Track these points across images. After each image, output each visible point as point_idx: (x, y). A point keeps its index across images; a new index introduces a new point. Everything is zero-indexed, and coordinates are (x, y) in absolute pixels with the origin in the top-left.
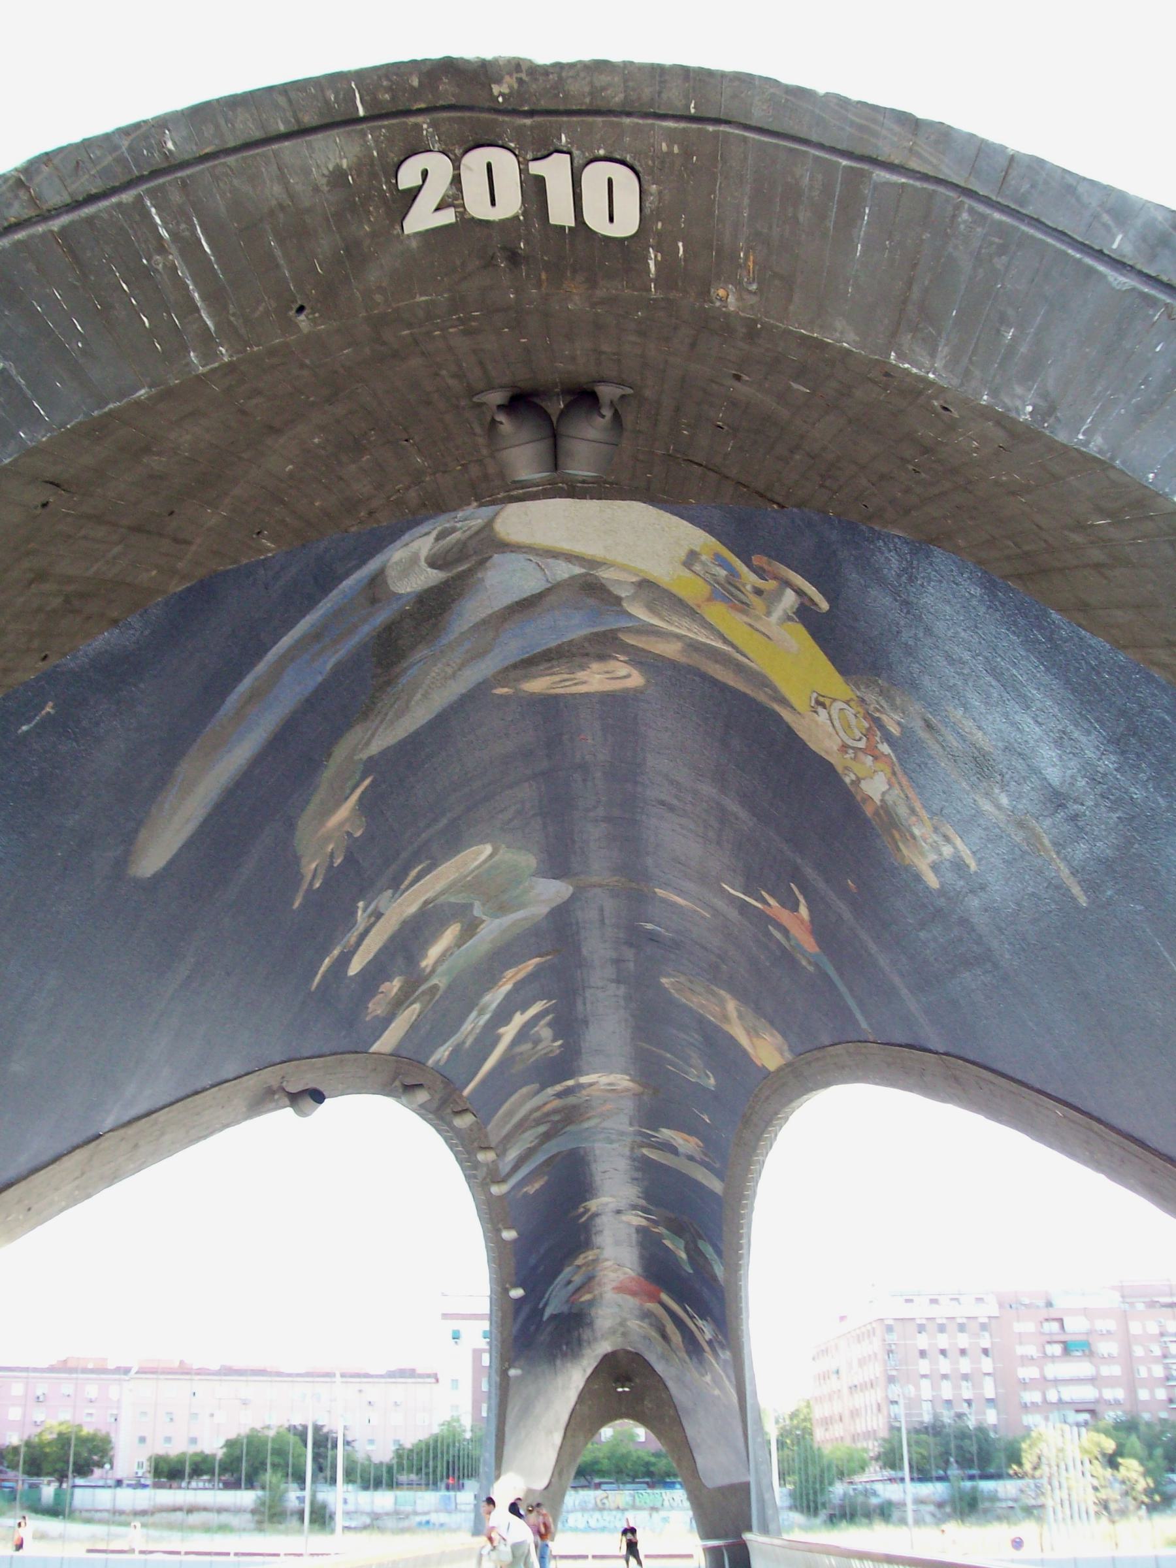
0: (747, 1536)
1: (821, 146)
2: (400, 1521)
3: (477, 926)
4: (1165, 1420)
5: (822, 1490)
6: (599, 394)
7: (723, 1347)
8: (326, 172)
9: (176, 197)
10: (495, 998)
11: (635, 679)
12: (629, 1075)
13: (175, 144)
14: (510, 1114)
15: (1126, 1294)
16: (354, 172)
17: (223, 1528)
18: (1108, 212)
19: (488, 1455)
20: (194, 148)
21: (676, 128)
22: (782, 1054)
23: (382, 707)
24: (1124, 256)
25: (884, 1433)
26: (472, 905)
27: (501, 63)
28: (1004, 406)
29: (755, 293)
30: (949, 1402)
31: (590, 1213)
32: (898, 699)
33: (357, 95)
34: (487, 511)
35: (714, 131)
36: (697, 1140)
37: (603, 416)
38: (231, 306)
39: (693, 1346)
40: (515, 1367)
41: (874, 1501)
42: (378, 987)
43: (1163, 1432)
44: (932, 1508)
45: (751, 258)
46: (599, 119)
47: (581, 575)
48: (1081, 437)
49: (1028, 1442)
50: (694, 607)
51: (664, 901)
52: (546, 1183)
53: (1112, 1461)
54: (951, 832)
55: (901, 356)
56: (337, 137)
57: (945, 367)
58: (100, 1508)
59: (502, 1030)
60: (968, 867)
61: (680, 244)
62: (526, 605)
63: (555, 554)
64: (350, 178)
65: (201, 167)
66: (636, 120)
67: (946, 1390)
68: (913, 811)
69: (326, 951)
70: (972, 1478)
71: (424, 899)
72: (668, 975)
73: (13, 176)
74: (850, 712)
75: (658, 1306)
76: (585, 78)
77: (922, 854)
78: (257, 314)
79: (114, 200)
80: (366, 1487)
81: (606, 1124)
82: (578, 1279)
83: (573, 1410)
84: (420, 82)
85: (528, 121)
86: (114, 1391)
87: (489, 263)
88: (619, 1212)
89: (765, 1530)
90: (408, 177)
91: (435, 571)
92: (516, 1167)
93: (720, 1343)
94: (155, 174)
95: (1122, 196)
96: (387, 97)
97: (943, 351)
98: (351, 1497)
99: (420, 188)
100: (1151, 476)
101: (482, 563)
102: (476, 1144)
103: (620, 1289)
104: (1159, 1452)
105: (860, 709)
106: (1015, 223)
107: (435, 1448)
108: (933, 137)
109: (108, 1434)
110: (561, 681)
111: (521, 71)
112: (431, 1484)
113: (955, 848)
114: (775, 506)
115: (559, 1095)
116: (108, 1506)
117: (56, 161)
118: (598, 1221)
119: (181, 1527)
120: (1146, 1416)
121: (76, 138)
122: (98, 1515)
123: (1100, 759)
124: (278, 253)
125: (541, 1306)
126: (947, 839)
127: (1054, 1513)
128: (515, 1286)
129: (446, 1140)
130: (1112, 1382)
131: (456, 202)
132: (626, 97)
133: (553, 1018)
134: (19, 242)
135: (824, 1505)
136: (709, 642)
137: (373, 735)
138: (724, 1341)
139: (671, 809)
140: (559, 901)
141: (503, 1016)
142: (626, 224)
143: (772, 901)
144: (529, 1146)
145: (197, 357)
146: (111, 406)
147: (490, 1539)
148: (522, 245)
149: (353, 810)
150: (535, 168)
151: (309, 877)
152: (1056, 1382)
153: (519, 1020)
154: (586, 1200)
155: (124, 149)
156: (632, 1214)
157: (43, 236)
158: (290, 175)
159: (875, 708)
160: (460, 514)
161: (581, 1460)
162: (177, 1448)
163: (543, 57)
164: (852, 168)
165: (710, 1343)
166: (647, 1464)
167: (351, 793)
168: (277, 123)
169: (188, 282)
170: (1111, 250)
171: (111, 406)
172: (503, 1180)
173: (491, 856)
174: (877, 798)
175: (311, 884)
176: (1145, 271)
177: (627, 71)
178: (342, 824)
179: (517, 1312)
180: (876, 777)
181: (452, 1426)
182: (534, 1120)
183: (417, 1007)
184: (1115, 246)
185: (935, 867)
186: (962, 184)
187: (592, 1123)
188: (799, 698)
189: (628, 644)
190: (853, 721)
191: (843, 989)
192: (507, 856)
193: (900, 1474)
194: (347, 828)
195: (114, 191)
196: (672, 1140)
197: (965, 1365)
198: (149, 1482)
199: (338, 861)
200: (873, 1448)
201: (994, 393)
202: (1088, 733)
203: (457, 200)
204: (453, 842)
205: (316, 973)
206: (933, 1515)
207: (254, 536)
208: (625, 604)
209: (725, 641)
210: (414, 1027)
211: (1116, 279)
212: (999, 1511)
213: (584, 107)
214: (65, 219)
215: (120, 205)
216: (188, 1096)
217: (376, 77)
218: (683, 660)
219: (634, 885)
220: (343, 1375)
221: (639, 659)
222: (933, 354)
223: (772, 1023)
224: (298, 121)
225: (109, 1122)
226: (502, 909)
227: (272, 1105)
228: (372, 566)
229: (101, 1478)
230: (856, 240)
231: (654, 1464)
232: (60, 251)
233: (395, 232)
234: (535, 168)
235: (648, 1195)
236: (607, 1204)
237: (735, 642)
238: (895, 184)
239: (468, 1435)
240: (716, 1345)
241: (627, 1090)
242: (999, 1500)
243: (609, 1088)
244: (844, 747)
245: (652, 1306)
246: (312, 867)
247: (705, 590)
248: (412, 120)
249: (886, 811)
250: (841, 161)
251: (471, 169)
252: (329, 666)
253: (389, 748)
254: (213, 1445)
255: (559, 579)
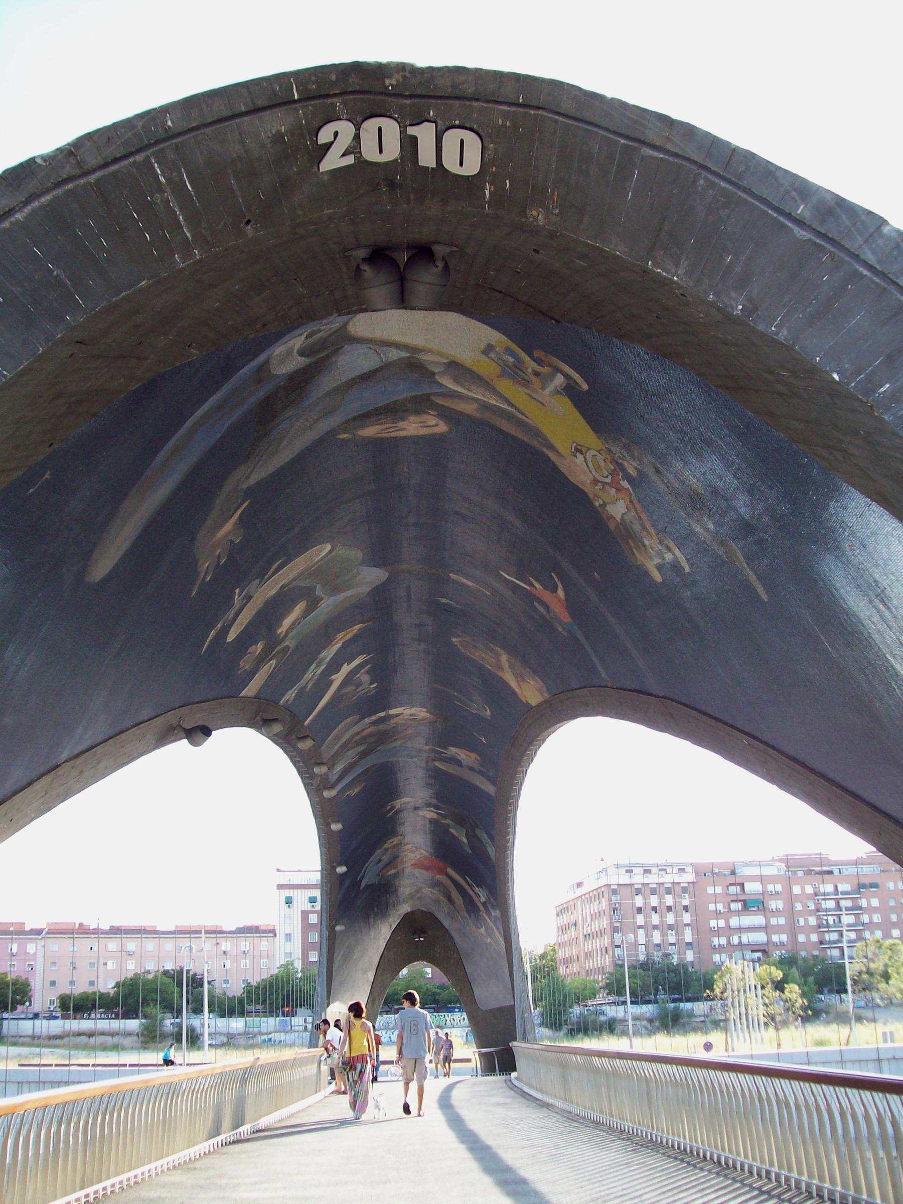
0: (513, 1044)
1: (607, 130)
2: (248, 1040)
3: (318, 602)
4: (817, 956)
5: (564, 1011)
6: (434, 251)
7: (494, 907)
8: (270, 135)
9: (171, 156)
10: (328, 654)
11: (442, 427)
12: (426, 708)
13: (172, 122)
14: (338, 738)
15: (790, 863)
16: (288, 134)
17: (116, 1048)
18: (795, 190)
19: (321, 989)
20: (185, 124)
21: (509, 110)
22: (542, 694)
23: (259, 452)
24: (805, 218)
25: (610, 969)
26: (315, 587)
27: (392, 66)
28: (724, 303)
29: (557, 215)
30: (658, 945)
31: (395, 809)
32: (636, 452)
33: (294, 86)
34: (345, 318)
35: (534, 114)
36: (476, 756)
37: (437, 267)
38: (203, 223)
39: (471, 907)
40: (339, 924)
41: (602, 1018)
42: (247, 649)
43: (815, 965)
44: (645, 1023)
45: (556, 193)
46: (457, 103)
47: (408, 358)
48: (773, 329)
49: (719, 973)
50: (489, 380)
51: (455, 582)
52: (363, 788)
53: (779, 986)
54: (672, 544)
55: (655, 264)
56: (279, 113)
57: (685, 274)
58: (23, 1034)
59: (333, 677)
60: (683, 569)
61: (508, 181)
62: (367, 377)
63: (389, 344)
64: (286, 138)
65: (189, 135)
66: (482, 104)
67: (657, 938)
68: (644, 528)
69: (212, 626)
70: (674, 1001)
71: (281, 584)
72: (457, 636)
73: (66, 148)
74: (600, 458)
75: (445, 877)
76: (448, 77)
77: (650, 558)
78: (219, 227)
79: (131, 160)
80: (223, 1016)
81: (409, 744)
82: (386, 858)
83: (382, 954)
84: (337, 78)
85: (408, 102)
86: (31, 948)
87: (376, 188)
88: (416, 808)
89: (525, 1040)
90: (324, 136)
91: (303, 358)
92: (340, 779)
93: (492, 904)
94: (158, 142)
95: (804, 181)
96: (314, 87)
97: (684, 263)
98: (212, 1022)
99: (332, 143)
100: (818, 358)
101: (336, 352)
102: (312, 761)
103: (418, 865)
104: (811, 979)
105: (608, 457)
106: (735, 190)
107: (277, 984)
108: (682, 131)
109: (27, 979)
110: (386, 429)
111: (406, 71)
112: (272, 1011)
113: (674, 554)
114: (553, 321)
115: (374, 723)
116: (30, 1032)
117: (95, 138)
118: (401, 816)
119: (85, 1047)
120: (803, 954)
121: (109, 122)
122: (22, 1040)
123: (778, 505)
124: (235, 187)
125: (359, 878)
126: (669, 549)
127: (735, 1025)
128: (340, 864)
129: (291, 758)
130: (779, 929)
131: (355, 151)
132: (476, 90)
133: (371, 667)
134: (69, 190)
135: (566, 1021)
136: (498, 404)
137: (252, 471)
138: (495, 903)
139: (464, 517)
140: (378, 583)
141: (334, 666)
142: (472, 166)
143: (537, 585)
144: (350, 761)
145: (179, 257)
146: (124, 294)
147: (327, 1049)
148: (398, 177)
149: (235, 524)
150: (411, 131)
151: (202, 575)
152: (740, 930)
153: (346, 669)
154: (393, 800)
155: (139, 127)
156: (427, 810)
157: (84, 186)
158: (247, 138)
159: (619, 456)
160: (325, 321)
161: (389, 990)
162: (81, 988)
163: (421, 62)
164: (627, 145)
165: (484, 904)
166: (434, 994)
167: (234, 514)
168: (241, 106)
169: (176, 210)
170: (798, 214)
171: (124, 294)
172: (332, 787)
173: (330, 552)
174: (618, 518)
175: (204, 578)
176: (818, 229)
177: (478, 73)
178: (227, 535)
179: (341, 884)
180: (618, 503)
181: (287, 967)
182: (355, 742)
183: (274, 662)
184: (799, 212)
185: (659, 568)
186: (701, 162)
187: (398, 743)
188: (563, 447)
189: (438, 404)
190: (602, 463)
191: (587, 647)
192: (343, 552)
193: (622, 999)
194: (230, 537)
195: (132, 154)
196: (456, 755)
197: (670, 919)
198: (59, 1015)
199: (223, 561)
200: (601, 980)
201: (717, 294)
202: (771, 488)
203: (356, 149)
204: (303, 544)
205: (206, 641)
206: (646, 1028)
207: (187, 348)
208: (437, 377)
209: (510, 404)
210: (271, 677)
211: (799, 232)
212: (694, 1024)
213: (447, 95)
214: (99, 174)
215: (135, 162)
216: (117, 735)
217: (307, 75)
218: (478, 416)
219: (433, 571)
220: (207, 932)
221: (445, 414)
222: (677, 265)
223: (535, 672)
224: (254, 103)
225: (65, 755)
226: (336, 590)
227: (173, 738)
228: (261, 358)
229: (23, 1012)
230: (628, 189)
231: (439, 994)
232: (95, 195)
233: (314, 170)
234: (411, 131)
235: (439, 796)
236: (408, 803)
237: (517, 405)
238: (656, 158)
239: (299, 975)
240: (488, 905)
241: (424, 719)
242: (696, 1016)
243: (411, 717)
244: (595, 482)
245: (439, 877)
246: (205, 567)
247: (498, 370)
248: (330, 101)
249: (624, 526)
250: (620, 140)
251: (367, 131)
252: (227, 425)
253: (262, 480)
254: (107, 986)
255: (390, 360)
